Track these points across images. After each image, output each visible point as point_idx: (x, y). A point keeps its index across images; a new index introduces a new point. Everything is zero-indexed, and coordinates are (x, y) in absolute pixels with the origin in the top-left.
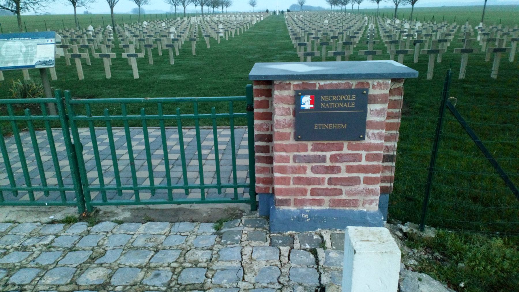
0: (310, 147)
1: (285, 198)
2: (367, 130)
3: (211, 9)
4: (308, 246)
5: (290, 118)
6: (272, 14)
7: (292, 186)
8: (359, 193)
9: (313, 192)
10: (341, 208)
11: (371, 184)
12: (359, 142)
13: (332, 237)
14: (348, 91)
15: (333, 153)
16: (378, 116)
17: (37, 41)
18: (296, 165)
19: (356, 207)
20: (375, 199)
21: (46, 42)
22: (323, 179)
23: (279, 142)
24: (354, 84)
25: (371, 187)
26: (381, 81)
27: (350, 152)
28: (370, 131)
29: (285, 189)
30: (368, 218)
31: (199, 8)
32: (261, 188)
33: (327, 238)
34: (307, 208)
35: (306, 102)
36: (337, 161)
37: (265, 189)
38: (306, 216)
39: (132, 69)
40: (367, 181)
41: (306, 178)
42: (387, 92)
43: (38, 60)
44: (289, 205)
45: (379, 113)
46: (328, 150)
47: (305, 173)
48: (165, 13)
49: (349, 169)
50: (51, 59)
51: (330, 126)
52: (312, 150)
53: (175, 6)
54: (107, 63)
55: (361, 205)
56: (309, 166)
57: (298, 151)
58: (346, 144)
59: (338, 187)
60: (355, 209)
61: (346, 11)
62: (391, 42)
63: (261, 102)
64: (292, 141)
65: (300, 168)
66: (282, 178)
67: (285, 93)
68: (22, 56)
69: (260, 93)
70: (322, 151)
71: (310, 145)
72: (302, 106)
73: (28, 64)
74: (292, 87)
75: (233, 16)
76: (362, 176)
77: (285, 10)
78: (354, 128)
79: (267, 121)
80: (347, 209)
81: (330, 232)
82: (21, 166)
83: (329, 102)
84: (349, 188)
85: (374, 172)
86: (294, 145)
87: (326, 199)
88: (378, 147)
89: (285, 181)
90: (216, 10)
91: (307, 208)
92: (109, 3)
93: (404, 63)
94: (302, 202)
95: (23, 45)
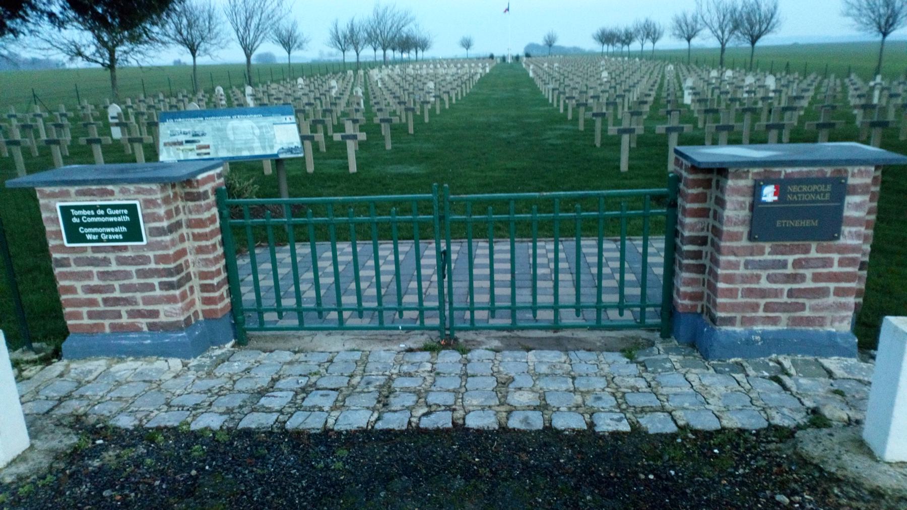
0: (768, 250)
1: (729, 315)
2: (843, 228)
3: (398, 55)
4: (766, 374)
5: (745, 213)
6: (499, 61)
7: (740, 300)
8: (827, 308)
9: (767, 308)
10: (803, 328)
11: (843, 296)
12: (832, 243)
13: (794, 363)
14: (823, 180)
15: (797, 256)
16: (856, 210)
17: (272, 119)
18: (748, 272)
19: (822, 326)
20: (847, 316)
21: (284, 121)
22: (782, 290)
23: (728, 244)
24: (829, 171)
25: (843, 300)
26: (863, 168)
27: (820, 255)
28: (846, 229)
29: (730, 303)
30: (839, 340)
31: (380, 52)
32: (686, 306)
33: (787, 363)
34: (758, 328)
35: (769, 194)
36: (802, 267)
37: (692, 306)
38: (758, 338)
39: (347, 158)
40: (839, 292)
41: (760, 289)
42: (869, 181)
43: (280, 147)
44: (733, 325)
45: (858, 206)
46: (792, 252)
47: (758, 283)
48: (309, 61)
49: (817, 278)
50: (296, 144)
51: (796, 223)
52: (769, 254)
53: (344, 51)
54: (351, 148)
55: (829, 323)
56: (764, 274)
57: (751, 255)
58: (814, 245)
59: (801, 300)
60: (821, 330)
61: (630, 55)
62: (707, 111)
63: (697, 195)
64: (744, 242)
65: (752, 276)
66: (727, 289)
67: (742, 183)
68: (257, 140)
69: (696, 184)
70: (783, 254)
71: (768, 247)
72: (763, 199)
73: (269, 152)
74: (750, 175)
75: (452, 65)
76: (832, 286)
77: (521, 52)
78: (828, 225)
79: (702, 219)
80: (811, 329)
81: (789, 358)
82: (644, 49)
83: (797, 193)
84: (814, 302)
85: (849, 281)
86: (748, 247)
87: (784, 316)
88: (854, 249)
89: (731, 293)
90: (405, 55)
91: (758, 328)
92: (245, 49)
93: (882, 146)
94: (752, 321)
95: (254, 125)
